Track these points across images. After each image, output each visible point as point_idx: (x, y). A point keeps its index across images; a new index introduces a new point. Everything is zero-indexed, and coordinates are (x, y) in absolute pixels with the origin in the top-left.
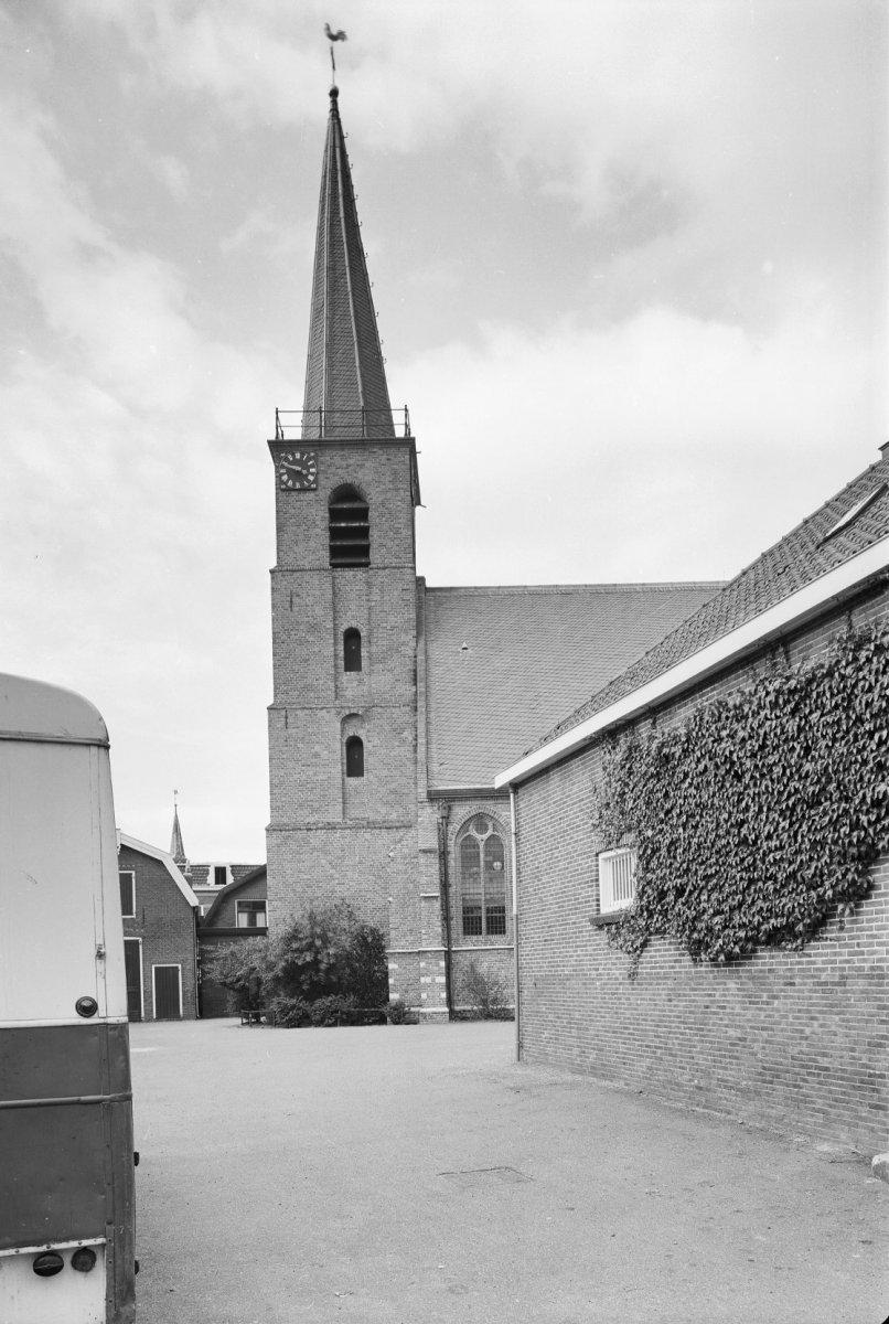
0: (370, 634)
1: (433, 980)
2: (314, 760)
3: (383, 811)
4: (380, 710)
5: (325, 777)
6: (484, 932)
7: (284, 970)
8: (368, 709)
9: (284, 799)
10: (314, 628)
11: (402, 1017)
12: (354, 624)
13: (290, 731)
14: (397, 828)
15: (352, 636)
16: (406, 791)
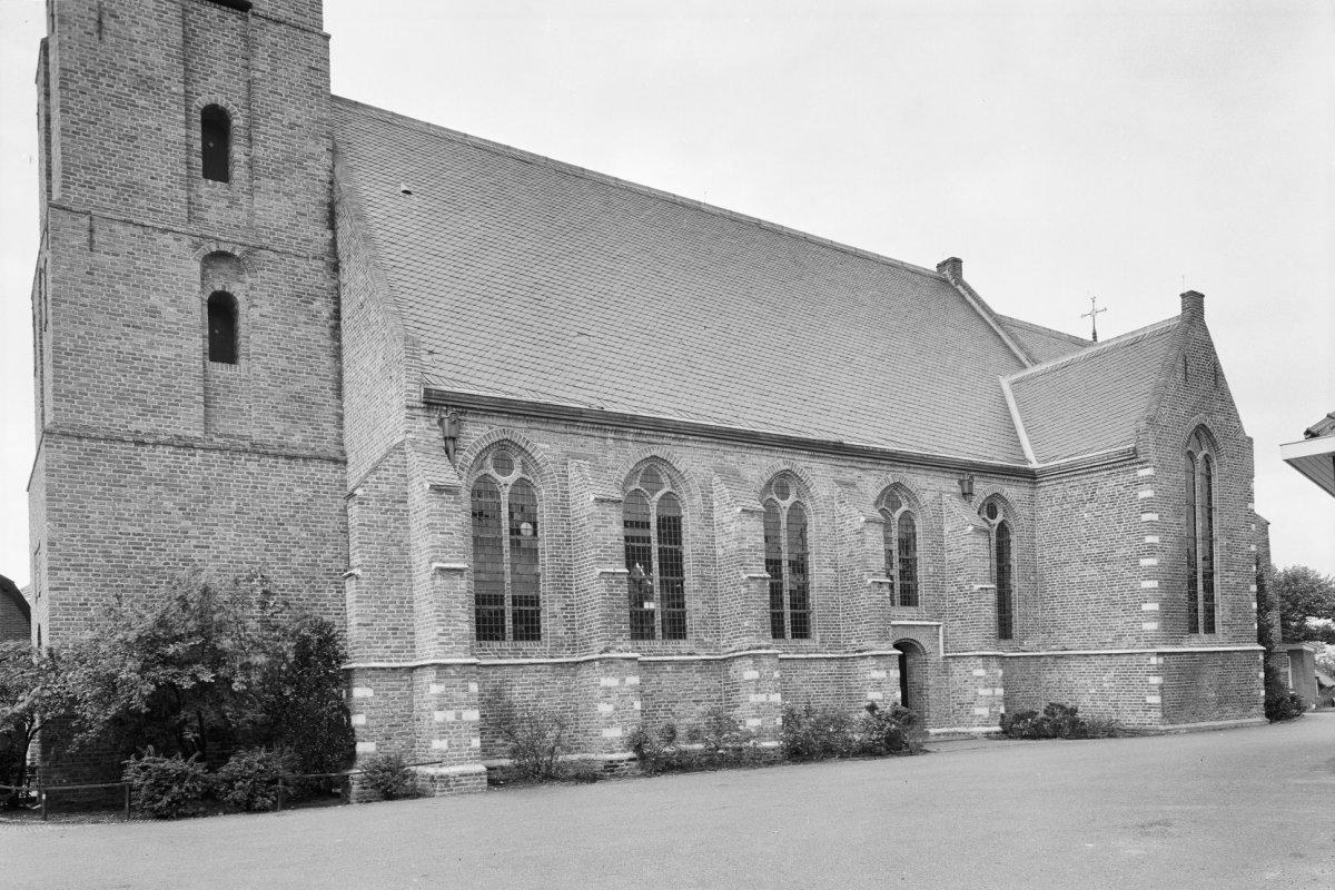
0: (252, 124)
1: (459, 716)
2: (147, 319)
3: (279, 427)
4: (273, 256)
5: (171, 353)
6: (658, 632)
7: (152, 700)
8: (251, 250)
9: (84, 380)
10: (146, 84)
11: (392, 784)
12: (221, 101)
13: (100, 258)
14: (305, 459)
15: (215, 124)
16: (319, 400)
